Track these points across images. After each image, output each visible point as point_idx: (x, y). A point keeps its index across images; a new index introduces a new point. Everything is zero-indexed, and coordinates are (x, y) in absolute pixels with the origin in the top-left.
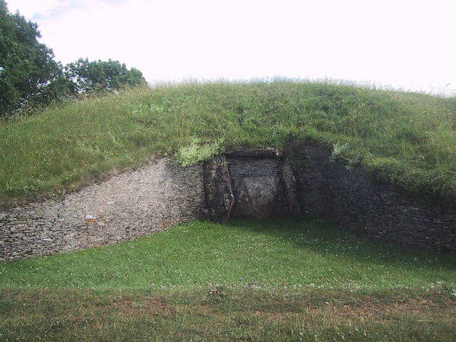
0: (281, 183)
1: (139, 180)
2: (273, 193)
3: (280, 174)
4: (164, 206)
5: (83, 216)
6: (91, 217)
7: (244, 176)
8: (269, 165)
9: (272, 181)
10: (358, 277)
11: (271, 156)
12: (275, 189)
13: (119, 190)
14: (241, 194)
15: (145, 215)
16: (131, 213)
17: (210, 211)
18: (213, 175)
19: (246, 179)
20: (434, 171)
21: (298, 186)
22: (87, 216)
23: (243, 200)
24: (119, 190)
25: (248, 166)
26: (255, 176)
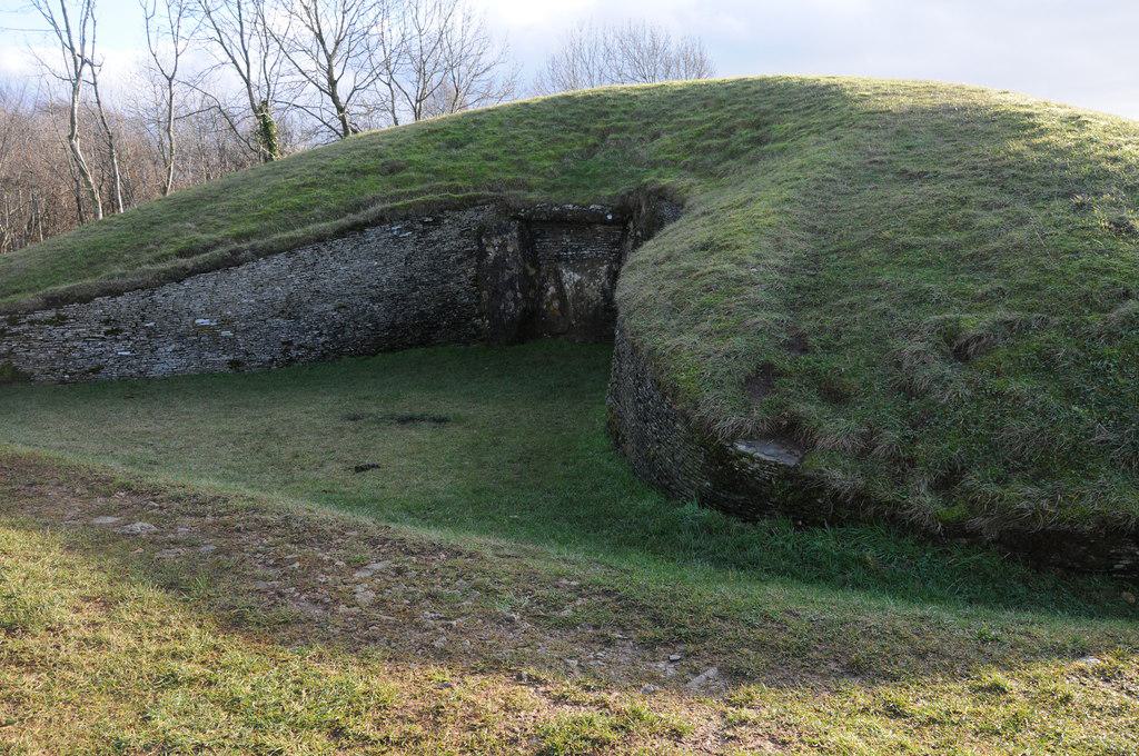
22: (197, 321)
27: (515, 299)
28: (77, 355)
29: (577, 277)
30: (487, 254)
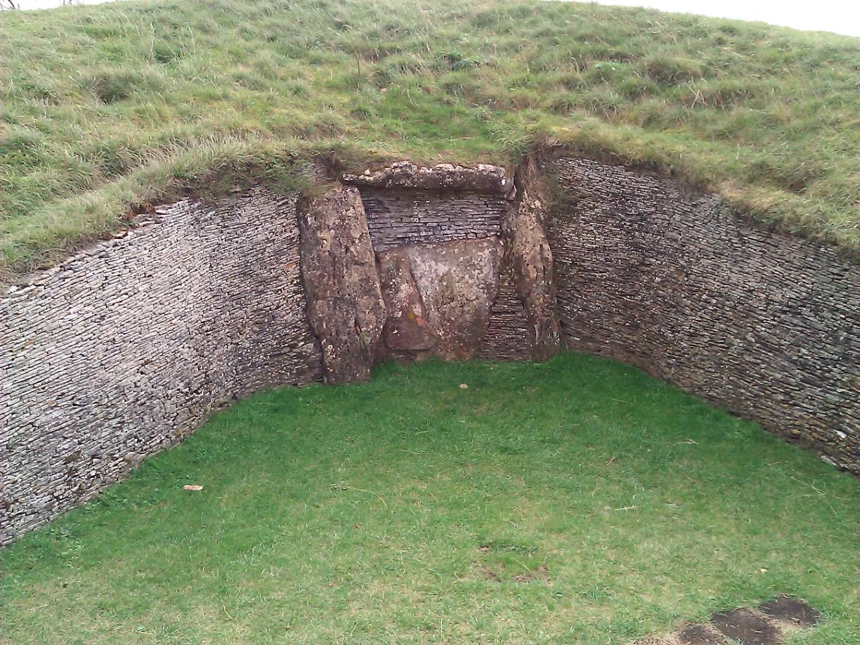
0: (510, 264)
1: (103, 287)
2: (488, 287)
3: (506, 236)
4: (186, 352)
7: (405, 242)
8: (476, 213)
9: (484, 255)
10: (720, 151)
11: (488, 189)
12: (492, 280)
13: (30, 334)
14: (402, 295)
15: (131, 397)
16: (79, 404)
17: (321, 349)
18: (327, 245)
19: (413, 254)
20: (560, 15)
21: (558, 274)
23: (406, 311)
24: (30, 334)
25: (419, 214)
26: (435, 243)
27: (375, 309)
29: (442, 269)
30: (319, 242)
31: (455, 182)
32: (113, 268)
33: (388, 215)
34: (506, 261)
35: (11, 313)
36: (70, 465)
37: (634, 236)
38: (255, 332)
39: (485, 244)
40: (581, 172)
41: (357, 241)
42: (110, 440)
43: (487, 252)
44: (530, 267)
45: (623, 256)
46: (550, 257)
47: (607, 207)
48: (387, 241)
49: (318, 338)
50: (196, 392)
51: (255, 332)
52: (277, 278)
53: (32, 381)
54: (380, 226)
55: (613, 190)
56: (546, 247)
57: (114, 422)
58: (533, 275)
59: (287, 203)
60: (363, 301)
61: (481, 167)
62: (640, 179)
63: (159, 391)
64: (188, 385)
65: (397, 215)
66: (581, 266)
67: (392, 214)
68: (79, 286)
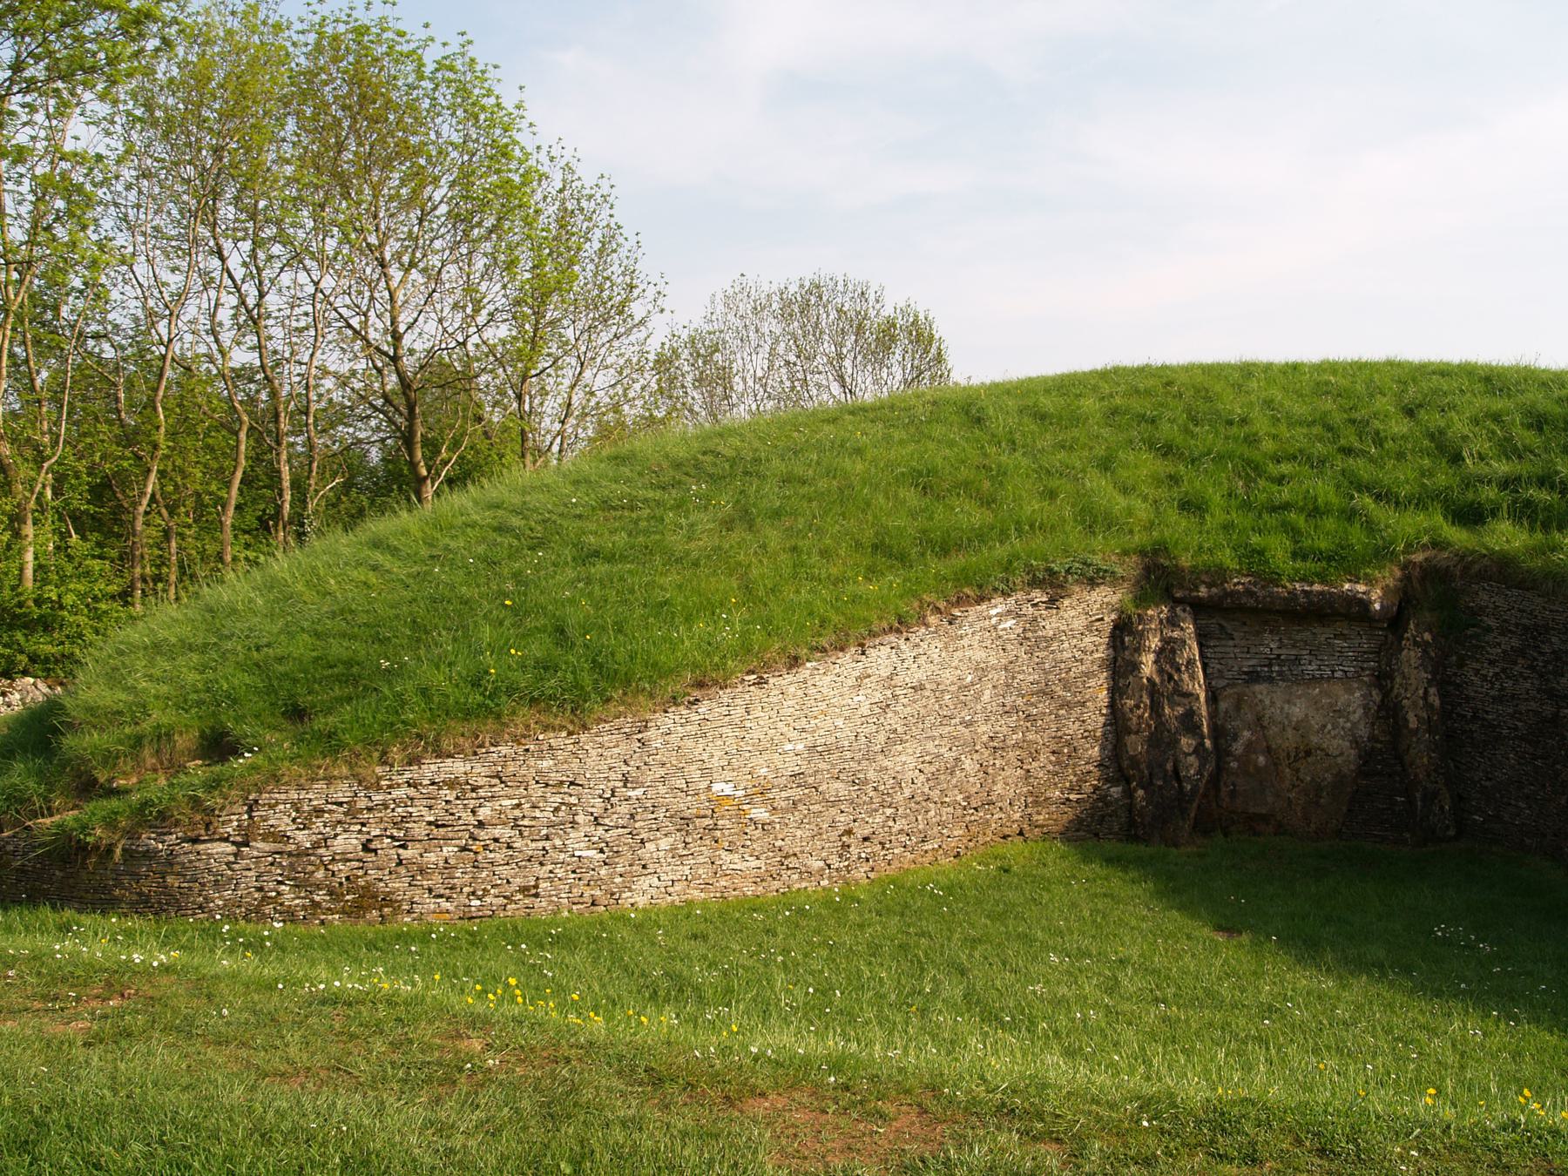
0: (1388, 712)
2: (1355, 742)
5: (703, 785)
6: (728, 789)
8: (1350, 646)
13: (823, 706)
19: (1260, 689)
28: (499, 857)
31: (1311, 603)
32: (903, 661)
33: (1231, 643)
34: (1382, 706)
35: (810, 683)
36: (844, 839)
37: (1548, 680)
38: (1051, 762)
39: (1356, 685)
40: (1486, 597)
41: (1183, 668)
42: (883, 827)
43: (1357, 694)
44: (737, 379)
45: (1533, 705)
46: (1437, 703)
47: (1515, 642)
48: (1229, 675)
49: (1128, 781)
50: (975, 809)
51: (1051, 762)
52: (1083, 704)
53: (819, 749)
54: (1220, 655)
55: (1524, 621)
56: (1432, 690)
57: (889, 811)
58: (1413, 723)
59: (1102, 619)
60: (1186, 743)
61: (1347, 586)
62: (1555, 608)
63: (935, 795)
64: (967, 798)
65: (1243, 643)
66: (1484, 719)
67: (1236, 642)
68: (869, 671)
